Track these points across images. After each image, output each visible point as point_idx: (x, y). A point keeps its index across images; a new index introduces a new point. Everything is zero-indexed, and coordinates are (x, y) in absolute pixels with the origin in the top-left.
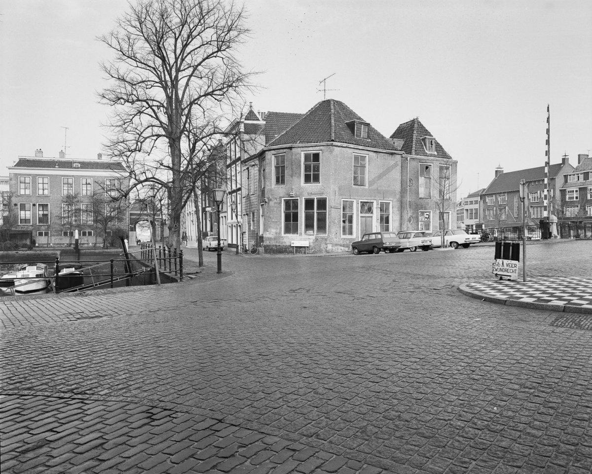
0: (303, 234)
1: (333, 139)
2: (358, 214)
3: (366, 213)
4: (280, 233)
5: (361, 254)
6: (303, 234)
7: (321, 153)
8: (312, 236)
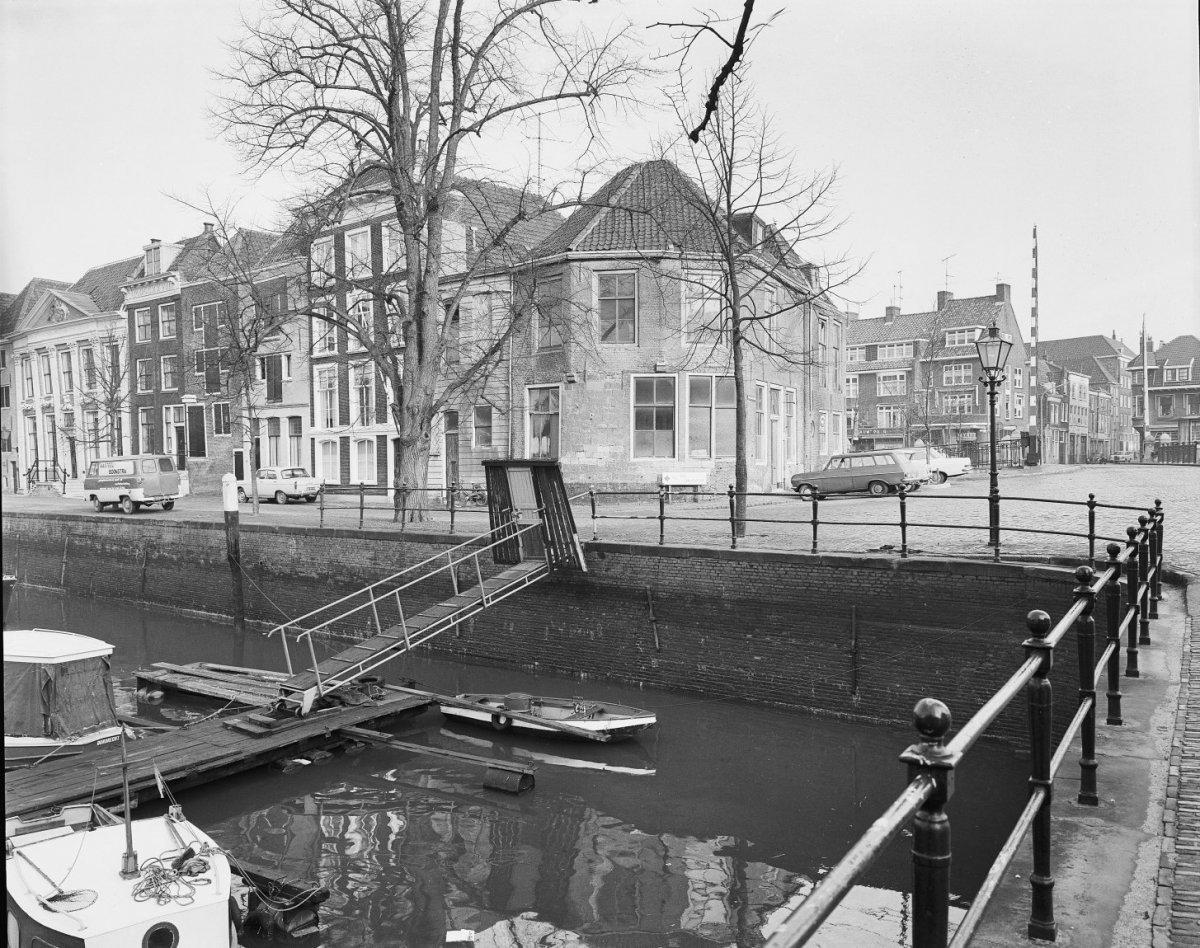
0: (687, 456)
4: (625, 455)
6: (687, 456)
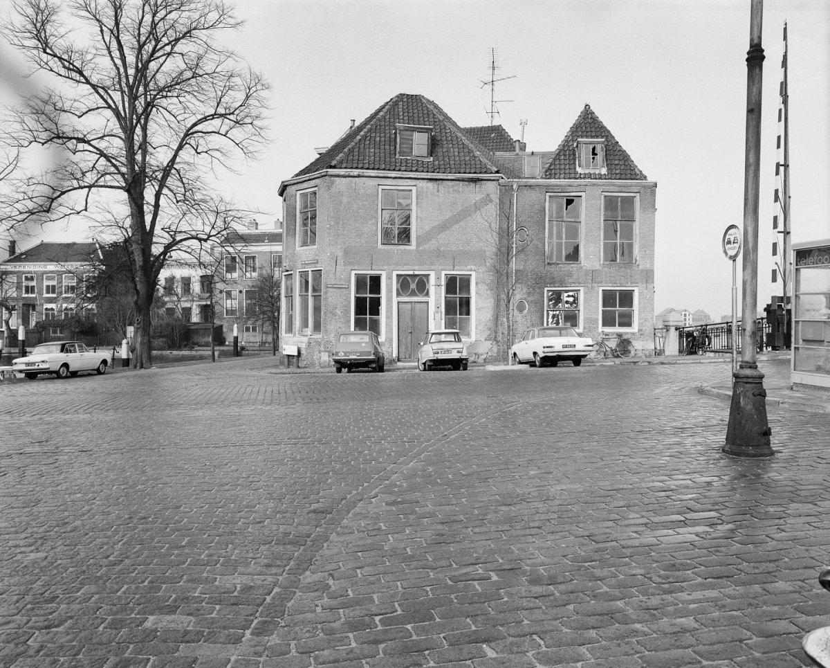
2: (391, 297)
5: (351, 372)
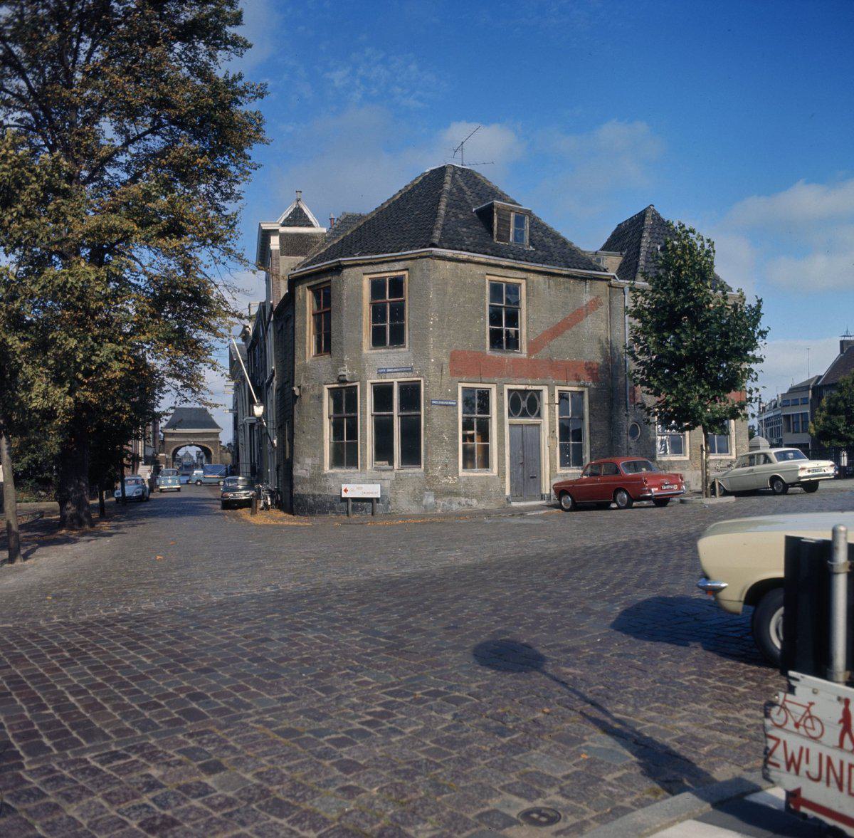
1: (436, 241)
2: (503, 419)
3: (524, 415)
4: (321, 467)
7: (407, 276)
8: (388, 473)
